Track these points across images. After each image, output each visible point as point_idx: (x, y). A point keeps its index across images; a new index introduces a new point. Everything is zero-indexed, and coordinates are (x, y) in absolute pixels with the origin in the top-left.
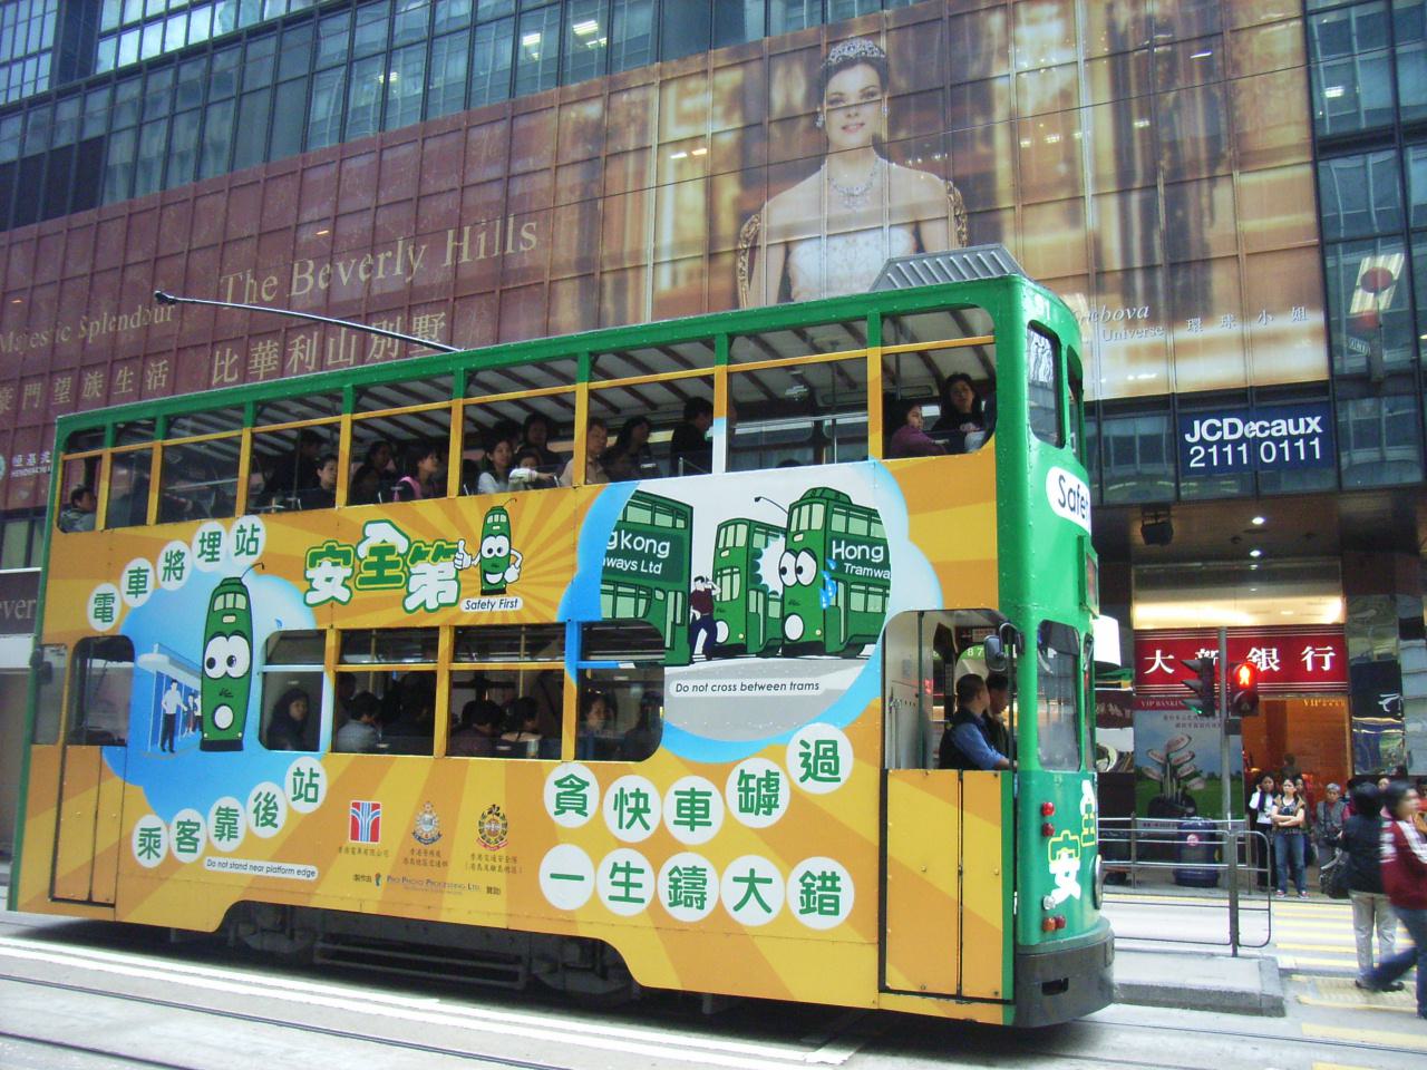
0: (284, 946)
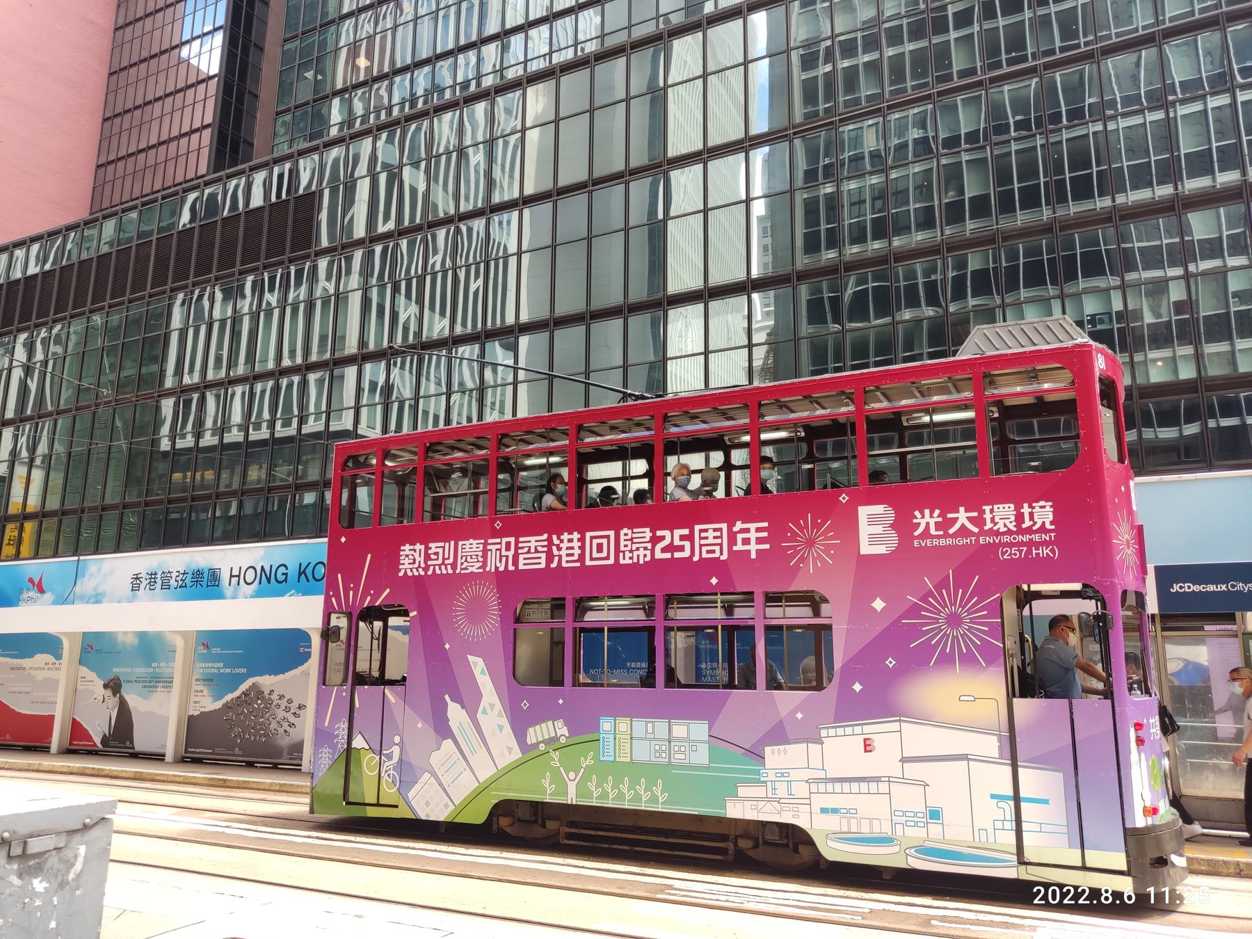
0: (538, 832)
